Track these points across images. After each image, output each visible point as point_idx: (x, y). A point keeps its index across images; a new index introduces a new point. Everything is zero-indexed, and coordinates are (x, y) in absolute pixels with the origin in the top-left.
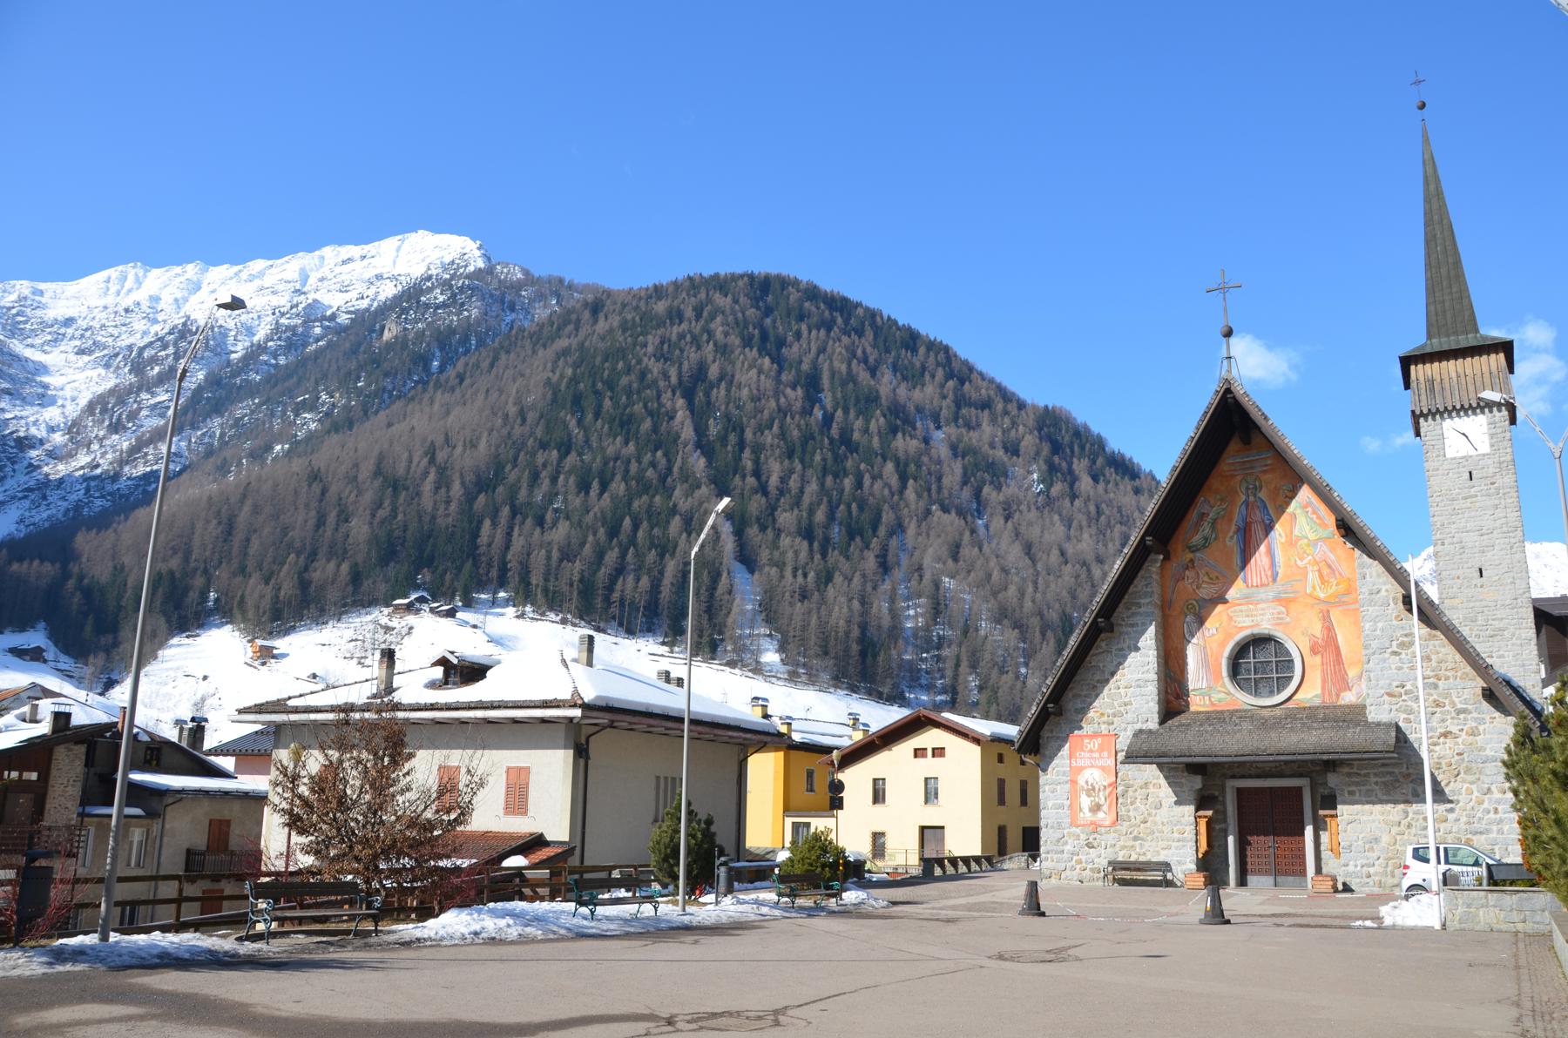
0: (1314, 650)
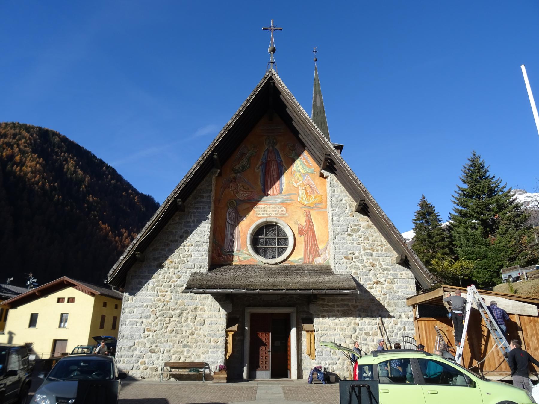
0: (301, 233)
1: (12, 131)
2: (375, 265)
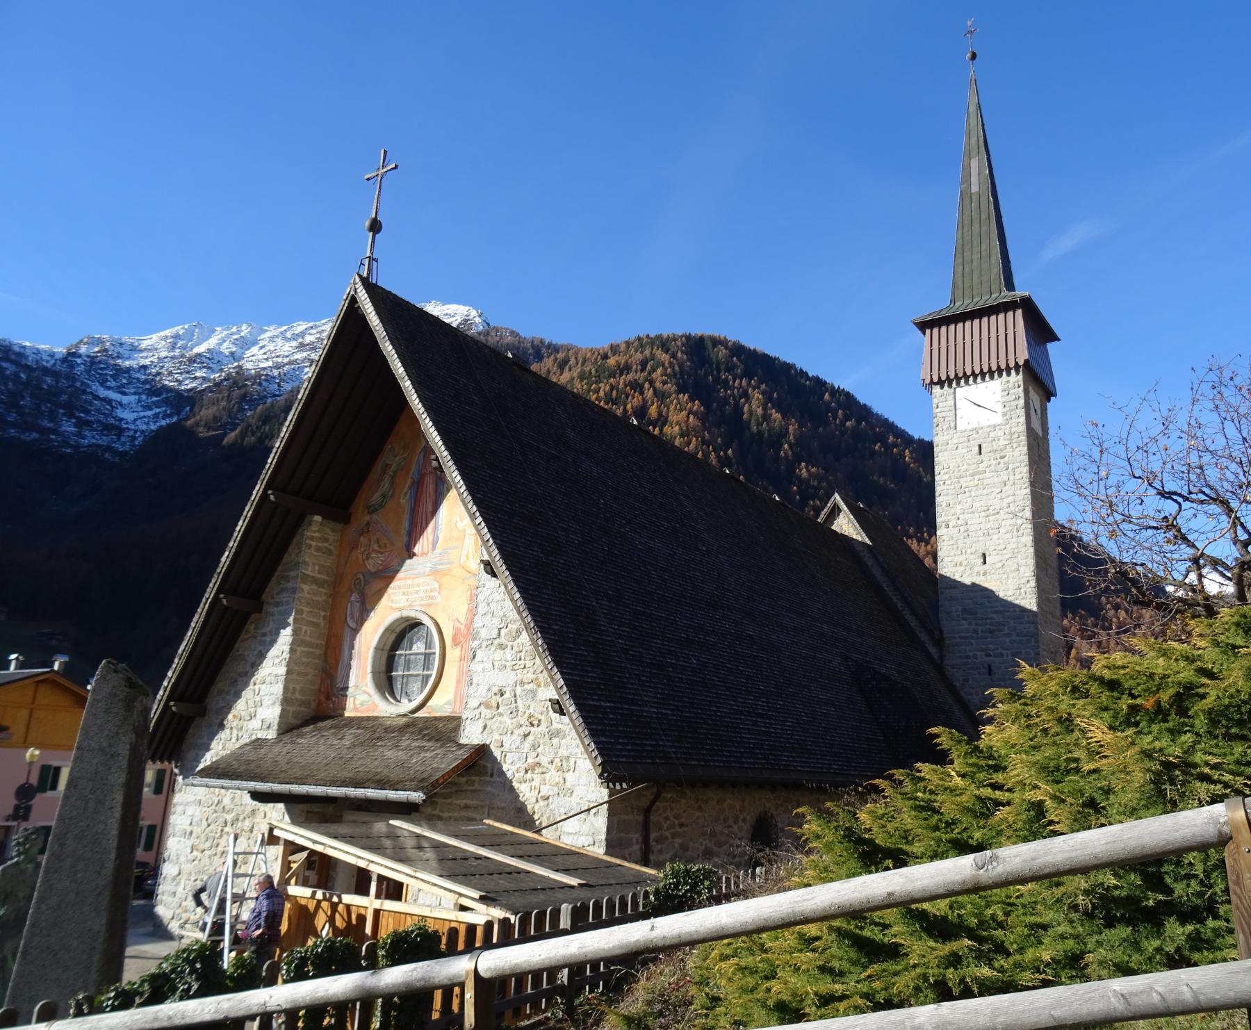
1: (639, 356)
2: (536, 722)
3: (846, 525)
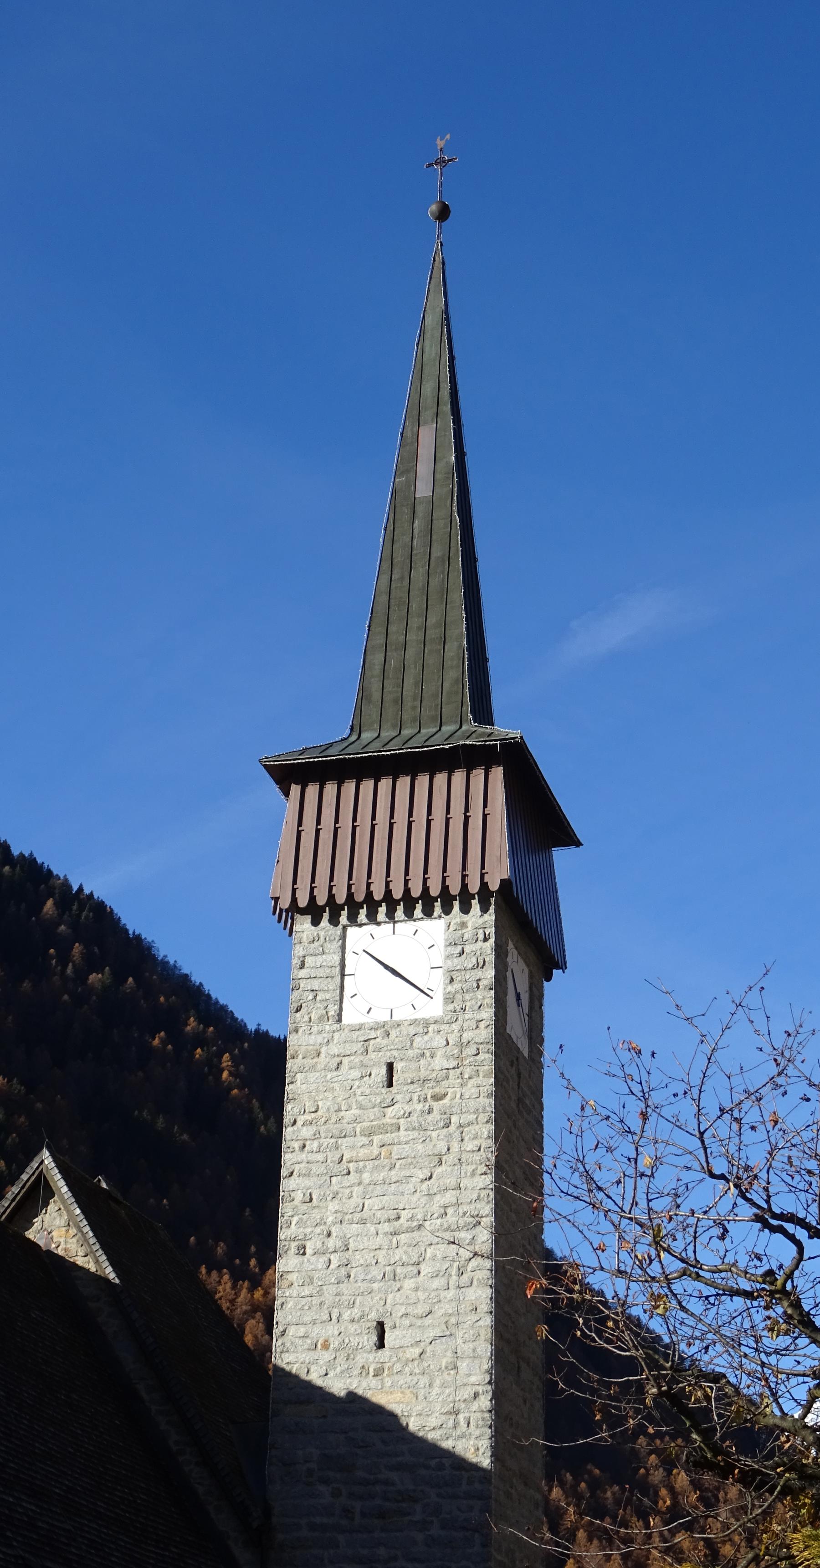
3: (61, 1230)
